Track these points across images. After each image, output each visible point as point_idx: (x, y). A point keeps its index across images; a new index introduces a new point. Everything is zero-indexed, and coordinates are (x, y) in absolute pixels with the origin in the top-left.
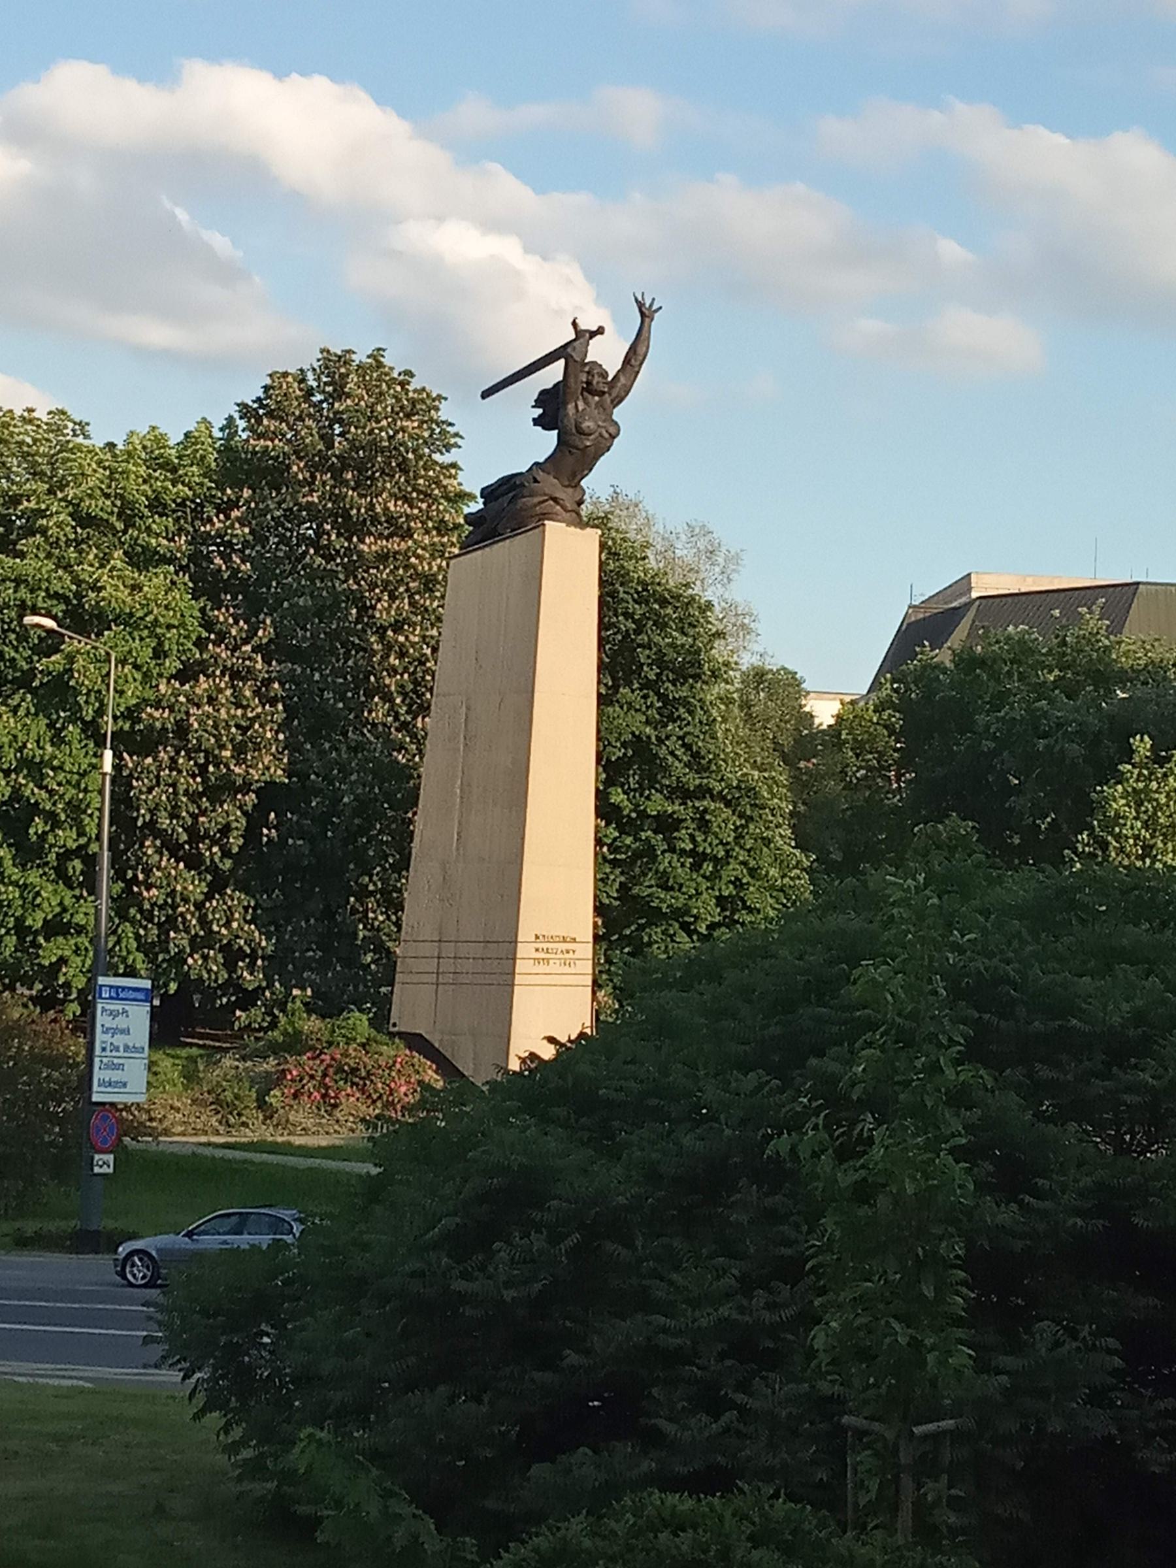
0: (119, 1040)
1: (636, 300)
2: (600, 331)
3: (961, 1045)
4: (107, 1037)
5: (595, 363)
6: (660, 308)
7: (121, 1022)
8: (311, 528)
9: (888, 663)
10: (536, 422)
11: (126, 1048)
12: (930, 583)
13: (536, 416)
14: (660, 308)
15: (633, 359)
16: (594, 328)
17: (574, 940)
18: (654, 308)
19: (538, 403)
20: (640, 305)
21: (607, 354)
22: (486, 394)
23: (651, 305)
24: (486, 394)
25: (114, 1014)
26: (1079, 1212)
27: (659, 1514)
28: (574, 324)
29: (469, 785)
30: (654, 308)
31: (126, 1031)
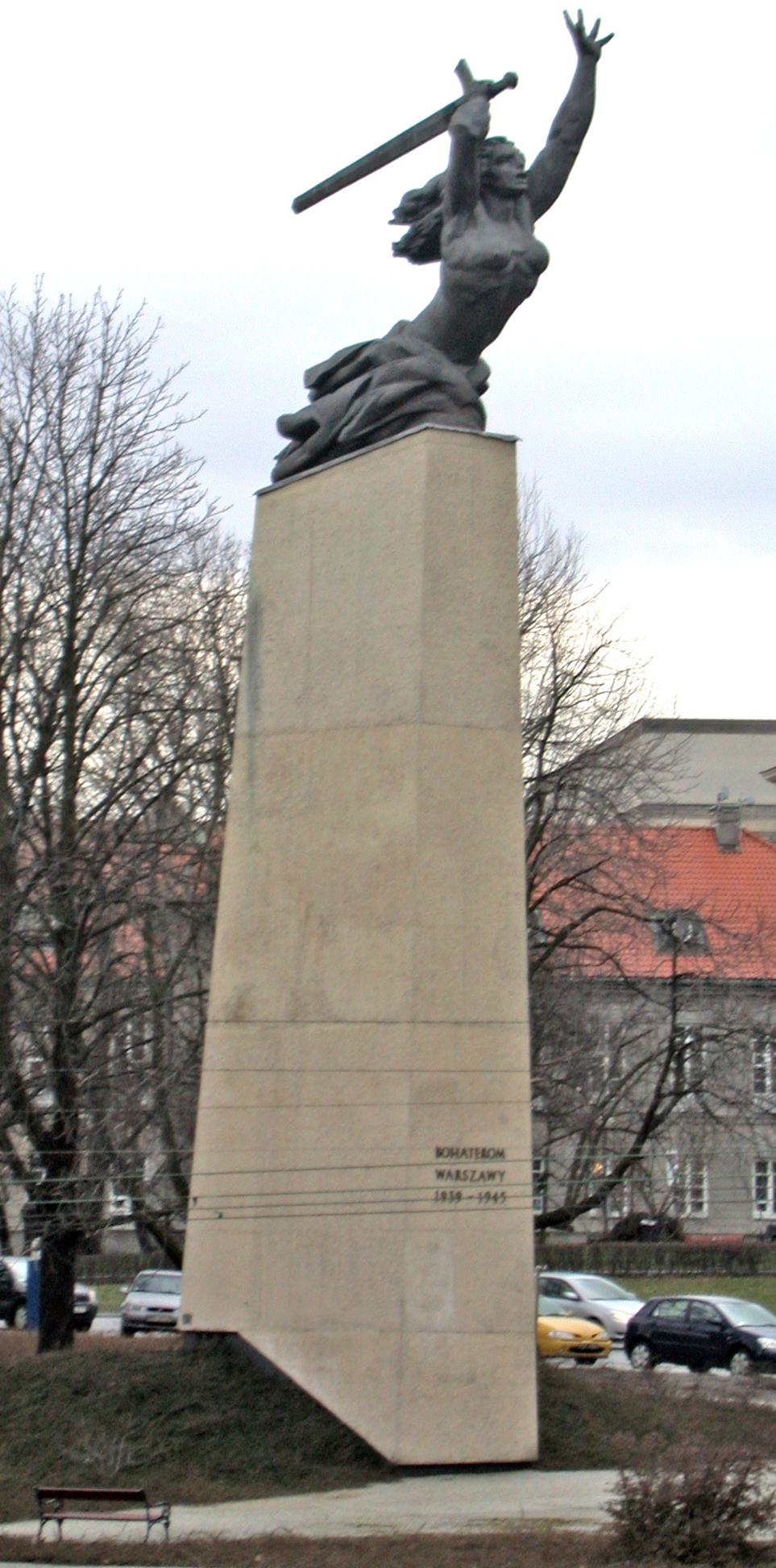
1: (569, 23)
2: (511, 81)
5: (501, 140)
6: (610, 37)
8: (691, 1444)
12: (230, 1327)
13: (398, 239)
14: (610, 37)
15: (573, 123)
16: (497, 77)
18: (599, 38)
20: (577, 31)
21: (522, 125)
22: (303, 203)
24: (303, 203)
28: (462, 70)
29: (624, 929)
30: (599, 38)
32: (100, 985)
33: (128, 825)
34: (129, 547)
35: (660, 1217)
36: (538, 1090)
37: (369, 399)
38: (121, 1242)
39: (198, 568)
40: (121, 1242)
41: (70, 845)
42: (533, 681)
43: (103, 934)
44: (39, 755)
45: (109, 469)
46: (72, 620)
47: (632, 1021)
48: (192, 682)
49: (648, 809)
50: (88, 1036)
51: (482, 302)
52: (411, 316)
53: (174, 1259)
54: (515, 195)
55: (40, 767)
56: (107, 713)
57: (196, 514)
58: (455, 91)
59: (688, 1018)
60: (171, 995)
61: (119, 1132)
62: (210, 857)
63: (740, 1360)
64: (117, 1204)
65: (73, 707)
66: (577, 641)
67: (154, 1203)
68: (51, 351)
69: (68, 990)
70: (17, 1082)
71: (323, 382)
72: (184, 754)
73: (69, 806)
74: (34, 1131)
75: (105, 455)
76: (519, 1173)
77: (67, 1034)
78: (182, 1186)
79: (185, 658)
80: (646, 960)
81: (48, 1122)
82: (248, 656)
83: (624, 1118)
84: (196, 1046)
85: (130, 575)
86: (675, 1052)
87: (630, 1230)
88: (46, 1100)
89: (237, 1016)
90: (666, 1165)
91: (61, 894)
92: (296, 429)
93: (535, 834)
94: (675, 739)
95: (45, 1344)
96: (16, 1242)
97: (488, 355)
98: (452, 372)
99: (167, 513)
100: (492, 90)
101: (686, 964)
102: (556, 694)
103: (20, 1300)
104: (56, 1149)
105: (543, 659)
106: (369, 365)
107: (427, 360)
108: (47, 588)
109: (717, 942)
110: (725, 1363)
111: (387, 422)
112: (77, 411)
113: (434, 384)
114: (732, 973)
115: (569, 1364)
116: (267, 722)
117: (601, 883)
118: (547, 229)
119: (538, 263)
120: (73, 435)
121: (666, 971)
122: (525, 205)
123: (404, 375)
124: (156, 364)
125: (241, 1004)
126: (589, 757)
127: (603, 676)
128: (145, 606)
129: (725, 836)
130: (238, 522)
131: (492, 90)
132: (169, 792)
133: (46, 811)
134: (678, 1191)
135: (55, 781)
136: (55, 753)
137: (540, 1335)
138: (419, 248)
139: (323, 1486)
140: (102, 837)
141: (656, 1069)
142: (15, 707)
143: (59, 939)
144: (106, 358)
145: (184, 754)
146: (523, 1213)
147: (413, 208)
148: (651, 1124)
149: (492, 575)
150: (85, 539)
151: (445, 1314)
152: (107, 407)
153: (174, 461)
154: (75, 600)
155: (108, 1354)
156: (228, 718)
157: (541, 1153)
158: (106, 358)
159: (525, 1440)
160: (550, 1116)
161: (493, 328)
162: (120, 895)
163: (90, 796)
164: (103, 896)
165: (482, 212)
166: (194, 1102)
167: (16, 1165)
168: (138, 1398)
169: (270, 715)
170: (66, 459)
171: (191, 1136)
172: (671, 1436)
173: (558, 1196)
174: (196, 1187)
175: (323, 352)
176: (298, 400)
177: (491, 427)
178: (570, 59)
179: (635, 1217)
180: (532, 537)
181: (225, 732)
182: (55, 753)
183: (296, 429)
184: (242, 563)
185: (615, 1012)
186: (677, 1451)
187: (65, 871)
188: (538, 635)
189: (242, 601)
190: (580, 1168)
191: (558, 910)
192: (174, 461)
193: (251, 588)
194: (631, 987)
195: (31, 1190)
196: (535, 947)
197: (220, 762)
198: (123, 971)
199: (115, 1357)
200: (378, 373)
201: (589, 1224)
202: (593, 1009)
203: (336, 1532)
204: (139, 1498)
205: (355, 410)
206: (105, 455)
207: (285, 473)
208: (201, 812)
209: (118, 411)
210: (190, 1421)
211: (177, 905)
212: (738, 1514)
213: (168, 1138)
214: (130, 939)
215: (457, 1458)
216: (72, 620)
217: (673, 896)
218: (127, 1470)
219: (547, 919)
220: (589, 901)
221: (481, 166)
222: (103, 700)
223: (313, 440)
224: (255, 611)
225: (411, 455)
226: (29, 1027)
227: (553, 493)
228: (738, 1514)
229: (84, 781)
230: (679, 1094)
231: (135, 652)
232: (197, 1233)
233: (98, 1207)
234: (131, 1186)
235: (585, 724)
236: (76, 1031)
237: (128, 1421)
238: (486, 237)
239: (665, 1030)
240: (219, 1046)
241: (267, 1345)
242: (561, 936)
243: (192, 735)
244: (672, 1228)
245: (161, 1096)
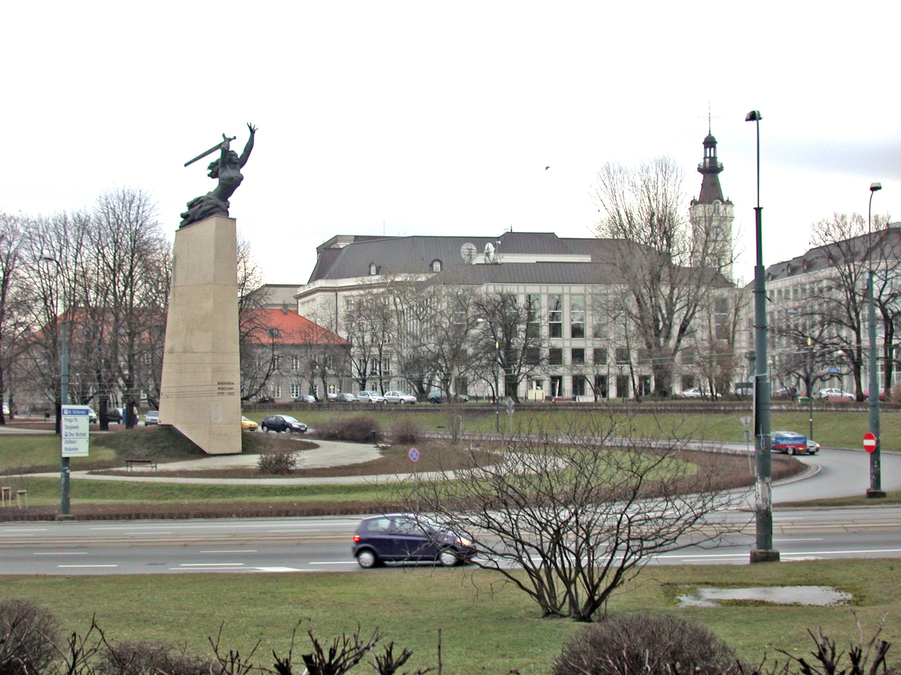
0: (73, 431)
2: (235, 138)
3: (330, 660)
4: (68, 430)
7: (74, 424)
10: (209, 175)
11: (77, 434)
12: (170, 423)
19: (210, 168)
20: (250, 127)
21: (237, 148)
22: (186, 165)
24: (186, 165)
25: (70, 421)
28: (224, 135)
31: (77, 427)
32: (139, 346)
33: (144, 309)
34: (145, 243)
35: (269, 398)
36: (241, 369)
37: (202, 209)
38: (144, 404)
39: (161, 248)
40: (144, 404)
41: (132, 313)
42: (240, 275)
43: (139, 333)
44: (124, 292)
45: (141, 225)
46: (132, 260)
47: (263, 353)
48: (160, 275)
49: (267, 305)
50: (136, 357)
51: (228, 187)
52: (212, 190)
53: (157, 408)
54: (235, 163)
55: (124, 294)
56: (140, 282)
57: (160, 236)
58: (222, 140)
59: (276, 353)
60: (156, 348)
61: (143, 380)
62: (164, 316)
63: (288, 429)
64: (144, 396)
65: (132, 280)
66: (250, 266)
67: (152, 395)
68: (127, 198)
69: (131, 346)
70: (120, 367)
71: (191, 206)
72: (158, 292)
73: (131, 304)
74: (124, 379)
75: (140, 222)
76: (237, 387)
77: (131, 356)
78: (158, 390)
79: (158, 269)
80: (266, 339)
81: (127, 377)
82: (173, 269)
83: (261, 375)
84: (161, 359)
85: (145, 250)
86: (273, 360)
87: (263, 401)
88: (126, 372)
89: (171, 352)
90: (271, 386)
91: (130, 324)
92: (184, 216)
93: (241, 310)
94: (272, 289)
95: (127, 428)
96: (120, 405)
97: (229, 199)
98: (221, 204)
99: (154, 235)
100: (230, 140)
101: (275, 340)
102: (245, 278)
103: (121, 418)
104: (129, 383)
105: (242, 270)
106: (202, 201)
107: (216, 201)
108: (126, 253)
109: (283, 335)
110: (284, 430)
111: (206, 215)
112: (133, 212)
113: (217, 206)
114: (286, 342)
115: (249, 431)
116: (178, 284)
117: (256, 321)
118: (243, 171)
119: (241, 179)
120: (132, 218)
121: (271, 341)
122: (238, 166)
123: (211, 204)
124: (152, 201)
125: (172, 349)
126: (253, 293)
127: (257, 273)
128: (149, 257)
129: (284, 311)
130: (170, 237)
131: (230, 140)
132: (155, 300)
133: (126, 305)
134: (274, 392)
135: (128, 298)
136: (128, 291)
137: (242, 424)
138: (213, 175)
139: (192, 459)
140: (139, 311)
141: (269, 365)
142: (119, 280)
143: (129, 334)
144: (140, 200)
145: (158, 292)
146: (238, 397)
147: (212, 166)
148: (268, 376)
149: (229, 250)
150: (135, 241)
151: (220, 420)
152: (140, 211)
153: (156, 224)
154: (132, 257)
155: (142, 430)
156: (169, 283)
157: (242, 384)
158: (140, 200)
159: (238, 447)
160: (244, 375)
161: (230, 193)
162: (143, 324)
163: (136, 301)
164: (140, 325)
165: (228, 167)
166: (161, 372)
167: (120, 387)
168: (149, 440)
169: (180, 281)
170: (131, 223)
171: (160, 380)
172: (272, 447)
173: (246, 393)
174: (162, 391)
175: (191, 199)
176: (185, 210)
177: (230, 216)
178: (249, 133)
179: (264, 398)
180: (240, 241)
181: (168, 286)
182: (128, 291)
183: (184, 216)
184: (172, 247)
185: (260, 351)
186: (273, 450)
187: (131, 318)
188: (241, 264)
189: (172, 256)
190: (251, 386)
191: (246, 328)
192: (156, 224)
193: (174, 252)
194: (263, 346)
195: (123, 392)
196: (240, 336)
197: (166, 293)
198: (144, 342)
199: (143, 431)
200: (204, 203)
201: (253, 400)
202: (254, 350)
203: (195, 469)
204: (149, 462)
205: (197, 213)
206: (140, 222)
207: (183, 226)
208: (162, 305)
209: (143, 212)
210: (161, 445)
211: (157, 326)
212: (287, 463)
213: (155, 380)
214: (146, 335)
215: (223, 452)
216: (132, 260)
217: (273, 324)
218: (147, 456)
219: (243, 330)
220: (253, 326)
221: (228, 157)
222: (140, 279)
223: (189, 219)
224: (175, 258)
225: (210, 225)
226: (122, 355)
227: (243, 233)
228: (287, 463)
229: (135, 298)
230: (274, 369)
231: (147, 268)
232: (162, 402)
233: (139, 396)
234: (146, 391)
235: (253, 285)
236: (133, 355)
237: (147, 445)
238: (229, 173)
239: (271, 355)
240: (167, 359)
241: (179, 427)
242: (246, 334)
243: (160, 288)
244: (272, 400)
245: (154, 371)
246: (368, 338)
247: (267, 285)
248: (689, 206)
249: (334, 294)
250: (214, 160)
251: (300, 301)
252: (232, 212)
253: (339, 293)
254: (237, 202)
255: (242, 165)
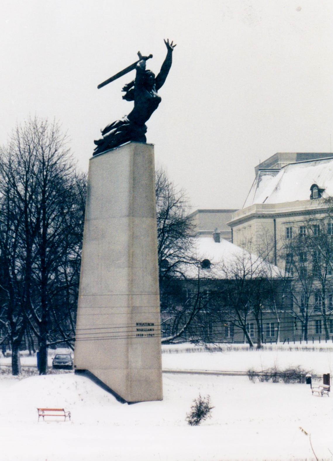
2: (151, 56)
9: (272, 158)
10: (124, 98)
16: (148, 55)
17: (153, 325)
18: (173, 45)
19: (125, 89)
20: (167, 44)
21: (154, 67)
22: (100, 86)
23: (171, 45)
24: (100, 86)
26: (227, 314)
27: (10, 165)
28: (139, 54)
30: (173, 45)
100: (146, 59)
118: (161, 93)
131: (146, 59)
142: (31, 212)
165: (145, 89)
178: (166, 51)
180: (157, 167)
207: (96, 153)
225: (124, 154)
246: (309, 266)
247: (200, 211)
248: (157, 231)
249: (271, 220)
250: (129, 81)
251: (235, 228)
252: (149, 136)
253: (278, 220)
254: (153, 125)
255: (159, 87)
